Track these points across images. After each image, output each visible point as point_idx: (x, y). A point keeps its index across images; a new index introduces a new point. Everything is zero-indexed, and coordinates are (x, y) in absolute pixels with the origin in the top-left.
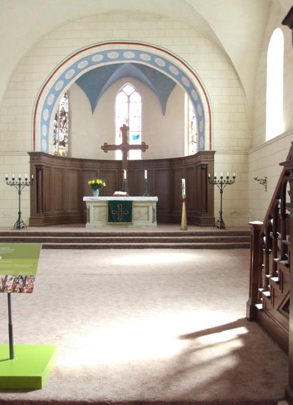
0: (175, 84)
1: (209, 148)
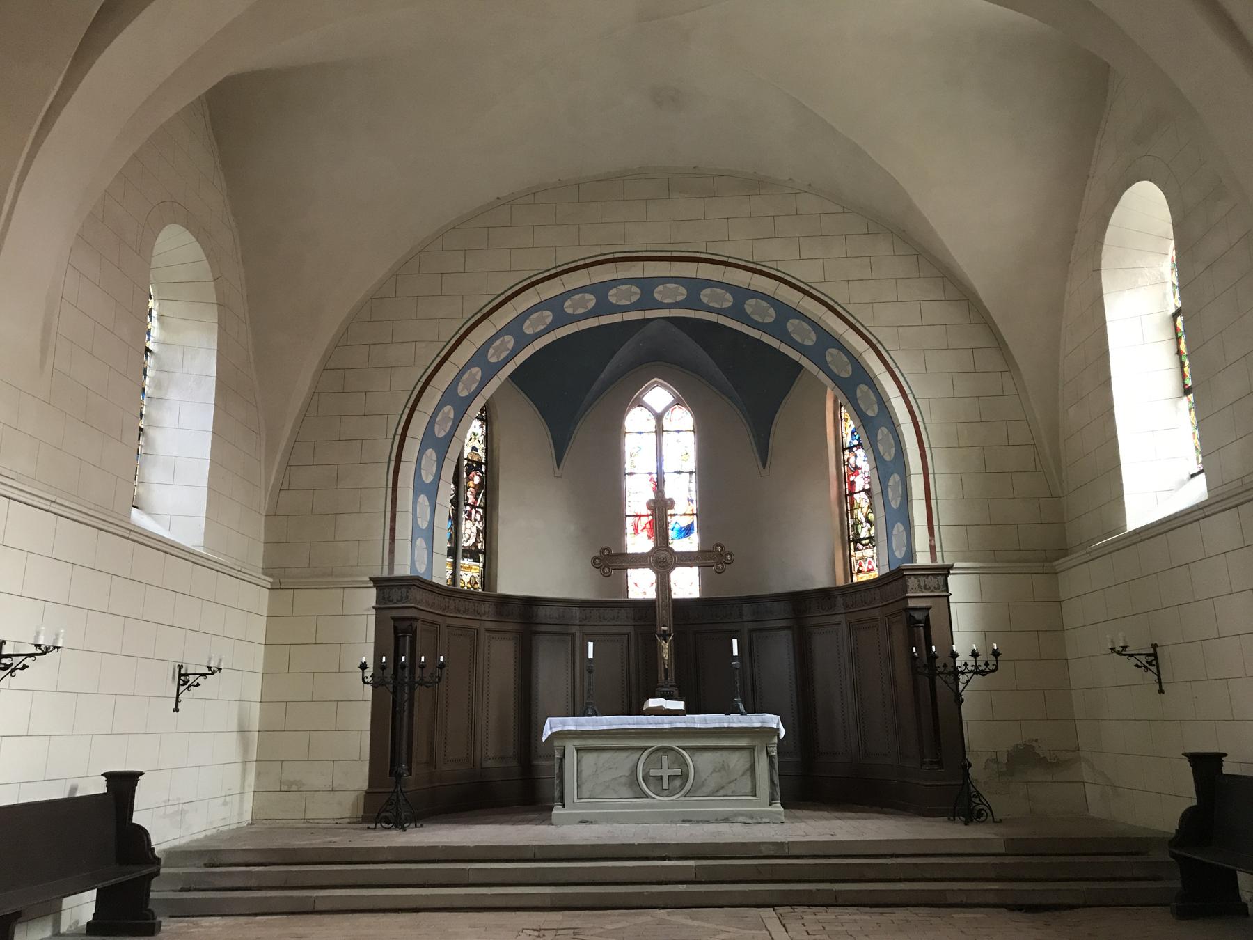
0: (800, 367)
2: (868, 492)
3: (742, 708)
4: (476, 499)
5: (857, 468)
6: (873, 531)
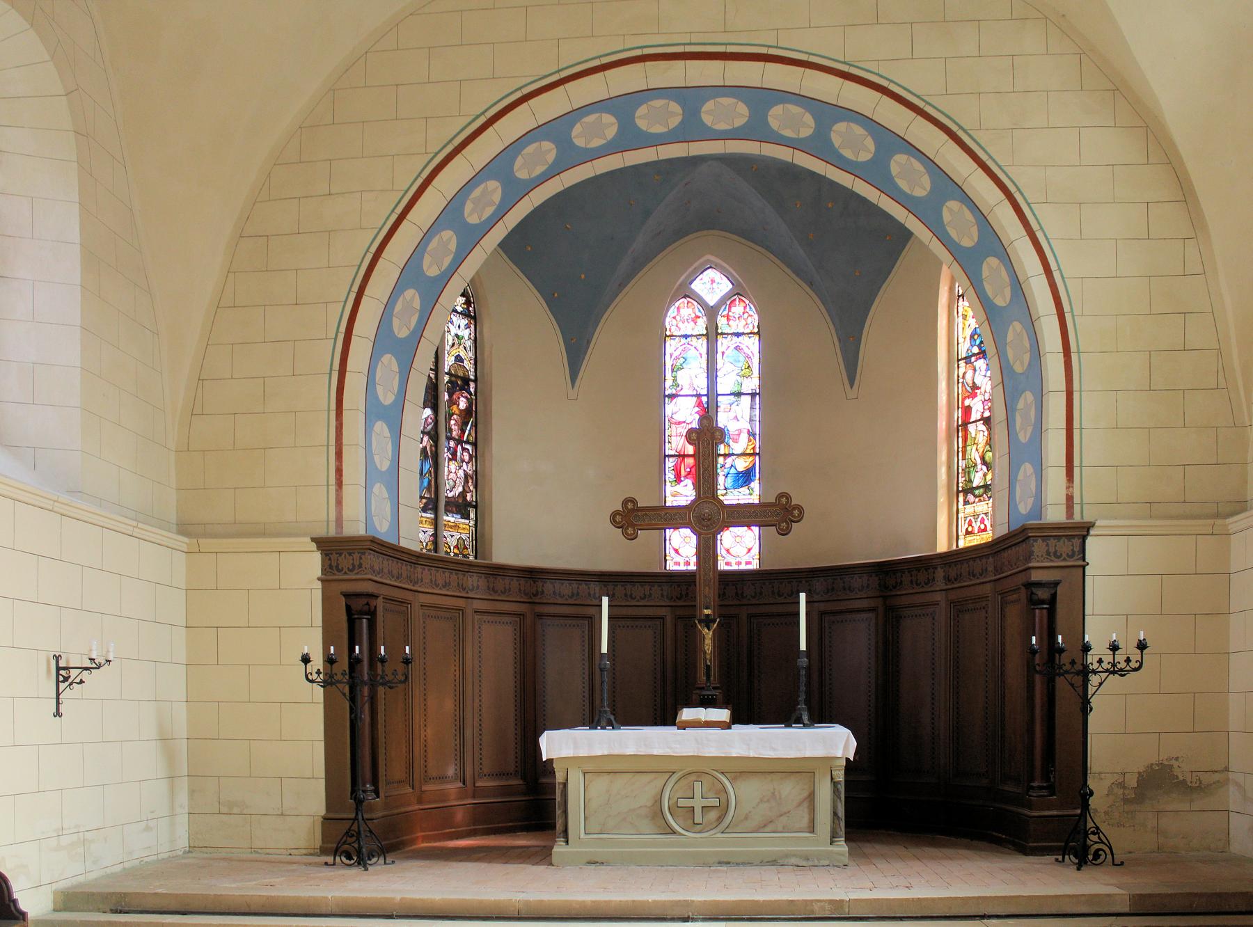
0: (905, 235)
1: (1063, 508)
2: (987, 421)
3: (805, 718)
4: (463, 432)
5: (975, 387)
6: (989, 477)
